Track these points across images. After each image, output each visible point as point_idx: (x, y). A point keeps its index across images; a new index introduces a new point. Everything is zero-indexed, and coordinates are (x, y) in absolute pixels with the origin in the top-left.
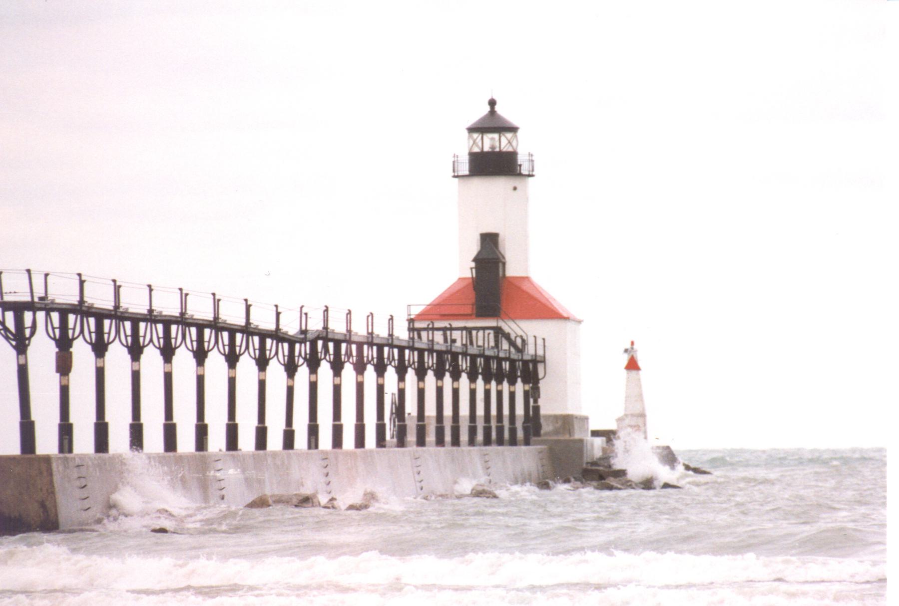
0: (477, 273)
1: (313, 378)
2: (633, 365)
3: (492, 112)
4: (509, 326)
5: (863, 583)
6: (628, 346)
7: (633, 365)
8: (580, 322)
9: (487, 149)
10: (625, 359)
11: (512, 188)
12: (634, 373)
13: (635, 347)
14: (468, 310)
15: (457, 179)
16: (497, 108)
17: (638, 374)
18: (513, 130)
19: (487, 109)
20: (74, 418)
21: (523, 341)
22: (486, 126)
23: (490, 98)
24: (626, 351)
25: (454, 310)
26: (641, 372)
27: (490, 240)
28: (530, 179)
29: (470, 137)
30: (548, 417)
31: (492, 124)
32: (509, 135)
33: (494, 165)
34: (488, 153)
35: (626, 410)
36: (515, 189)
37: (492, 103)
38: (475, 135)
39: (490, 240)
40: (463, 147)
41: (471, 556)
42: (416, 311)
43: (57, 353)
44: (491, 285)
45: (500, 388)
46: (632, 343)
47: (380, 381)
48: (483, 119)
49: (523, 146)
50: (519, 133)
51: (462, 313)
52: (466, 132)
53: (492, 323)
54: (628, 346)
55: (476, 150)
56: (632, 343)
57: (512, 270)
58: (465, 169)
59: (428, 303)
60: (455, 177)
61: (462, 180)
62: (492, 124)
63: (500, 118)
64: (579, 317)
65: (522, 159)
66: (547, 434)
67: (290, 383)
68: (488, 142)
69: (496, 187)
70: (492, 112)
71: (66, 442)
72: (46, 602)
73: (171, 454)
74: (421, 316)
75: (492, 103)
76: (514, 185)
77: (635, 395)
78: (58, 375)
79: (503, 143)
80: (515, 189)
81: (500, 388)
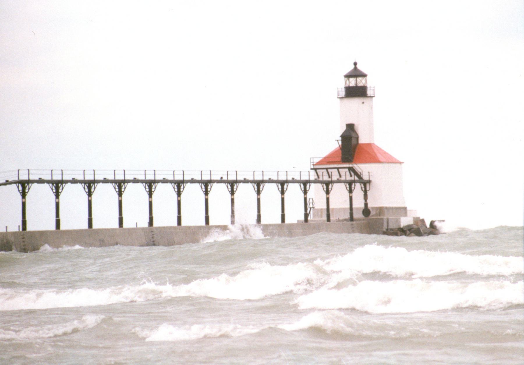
0: (342, 143)
1: (57, 200)
3: (356, 68)
5: (476, 277)
8: (400, 163)
14: (339, 159)
16: (358, 66)
19: (353, 67)
22: (351, 74)
27: (351, 127)
30: (373, 208)
31: (356, 73)
34: (353, 87)
36: (363, 103)
37: (355, 64)
39: (351, 127)
40: (341, 84)
42: (317, 160)
44: (351, 147)
47: (90, 199)
48: (352, 71)
49: (370, 83)
53: (347, 165)
55: (347, 86)
57: (363, 140)
58: (343, 93)
62: (356, 73)
64: (402, 161)
66: (373, 216)
68: (352, 82)
69: (355, 102)
70: (356, 68)
72: (259, 361)
74: (319, 163)
75: (355, 64)
76: (363, 101)
79: (361, 82)
80: (363, 103)
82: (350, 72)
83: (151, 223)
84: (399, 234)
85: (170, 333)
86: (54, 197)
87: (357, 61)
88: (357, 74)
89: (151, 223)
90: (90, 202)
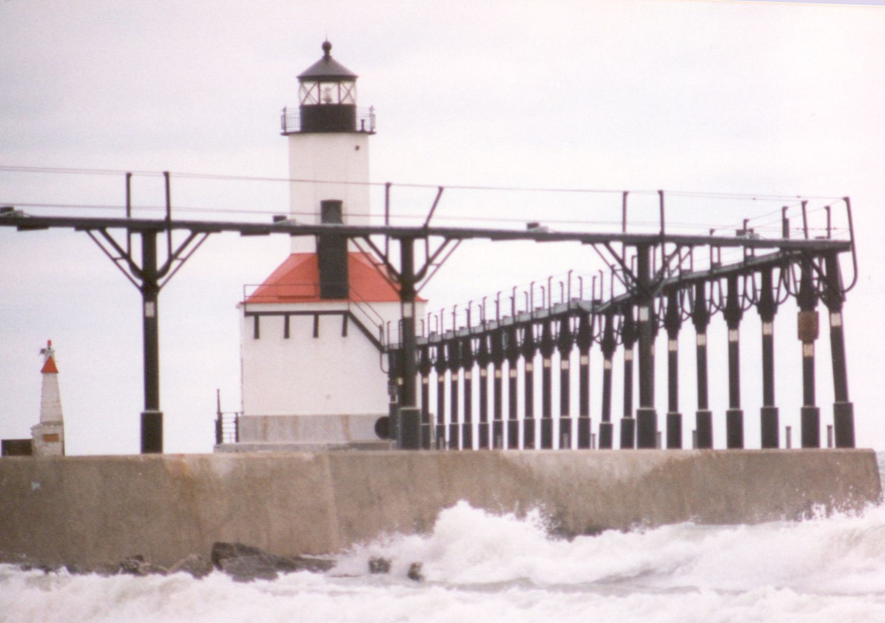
2: (50, 368)
3: (327, 58)
4: (355, 310)
6: (45, 346)
7: (50, 368)
9: (335, 101)
10: (40, 361)
11: (353, 148)
12: (51, 376)
13: (53, 347)
14: (310, 291)
15: (286, 138)
16: (333, 53)
17: (56, 377)
18: (351, 78)
19: (321, 54)
20: (779, 401)
21: (381, 329)
22: (314, 74)
23: (323, 40)
24: (43, 351)
25: (284, 292)
26: (58, 375)
28: (371, 137)
29: (302, 86)
31: (326, 72)
32: (348, 85)
33: (328, 120)
35: (42, 417)
36: (357, 148)
37: (327, 47)
38: (308, 86)
40: (293, 98)
41: (284, 579)
43: (799, 314)
45: (425, 381)
46: (49, 343)
48: (317, 66)
49: (363, 97)
50: (358, 82)
51: (300, 294)
52: (296, 83)
54: (45, 346)
56: (49, 343)
58: (295, 124)
59: (261, 282)
60: (285, 134)
61: (293, 137)
62: (326, 72)
63: (336, 65)
65: (361, 114)
67: (608, 366)
68: (316, 94)
70: (327, 58)
71: (566, 439)
73: (736, 451)
75: (327, 47)
77: (51, 399)
78: (800, 343)
79: (333, 93)
81: (455, 378)
82: (308, 71)
83: (152, 430)
84: (503, 509)
85: (533, 519)
86: (138, 296)
87: (330, 40)
88: (330, 72)
89: (152, 430)
90: (150, 328)
